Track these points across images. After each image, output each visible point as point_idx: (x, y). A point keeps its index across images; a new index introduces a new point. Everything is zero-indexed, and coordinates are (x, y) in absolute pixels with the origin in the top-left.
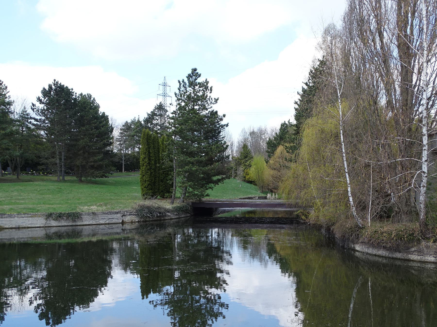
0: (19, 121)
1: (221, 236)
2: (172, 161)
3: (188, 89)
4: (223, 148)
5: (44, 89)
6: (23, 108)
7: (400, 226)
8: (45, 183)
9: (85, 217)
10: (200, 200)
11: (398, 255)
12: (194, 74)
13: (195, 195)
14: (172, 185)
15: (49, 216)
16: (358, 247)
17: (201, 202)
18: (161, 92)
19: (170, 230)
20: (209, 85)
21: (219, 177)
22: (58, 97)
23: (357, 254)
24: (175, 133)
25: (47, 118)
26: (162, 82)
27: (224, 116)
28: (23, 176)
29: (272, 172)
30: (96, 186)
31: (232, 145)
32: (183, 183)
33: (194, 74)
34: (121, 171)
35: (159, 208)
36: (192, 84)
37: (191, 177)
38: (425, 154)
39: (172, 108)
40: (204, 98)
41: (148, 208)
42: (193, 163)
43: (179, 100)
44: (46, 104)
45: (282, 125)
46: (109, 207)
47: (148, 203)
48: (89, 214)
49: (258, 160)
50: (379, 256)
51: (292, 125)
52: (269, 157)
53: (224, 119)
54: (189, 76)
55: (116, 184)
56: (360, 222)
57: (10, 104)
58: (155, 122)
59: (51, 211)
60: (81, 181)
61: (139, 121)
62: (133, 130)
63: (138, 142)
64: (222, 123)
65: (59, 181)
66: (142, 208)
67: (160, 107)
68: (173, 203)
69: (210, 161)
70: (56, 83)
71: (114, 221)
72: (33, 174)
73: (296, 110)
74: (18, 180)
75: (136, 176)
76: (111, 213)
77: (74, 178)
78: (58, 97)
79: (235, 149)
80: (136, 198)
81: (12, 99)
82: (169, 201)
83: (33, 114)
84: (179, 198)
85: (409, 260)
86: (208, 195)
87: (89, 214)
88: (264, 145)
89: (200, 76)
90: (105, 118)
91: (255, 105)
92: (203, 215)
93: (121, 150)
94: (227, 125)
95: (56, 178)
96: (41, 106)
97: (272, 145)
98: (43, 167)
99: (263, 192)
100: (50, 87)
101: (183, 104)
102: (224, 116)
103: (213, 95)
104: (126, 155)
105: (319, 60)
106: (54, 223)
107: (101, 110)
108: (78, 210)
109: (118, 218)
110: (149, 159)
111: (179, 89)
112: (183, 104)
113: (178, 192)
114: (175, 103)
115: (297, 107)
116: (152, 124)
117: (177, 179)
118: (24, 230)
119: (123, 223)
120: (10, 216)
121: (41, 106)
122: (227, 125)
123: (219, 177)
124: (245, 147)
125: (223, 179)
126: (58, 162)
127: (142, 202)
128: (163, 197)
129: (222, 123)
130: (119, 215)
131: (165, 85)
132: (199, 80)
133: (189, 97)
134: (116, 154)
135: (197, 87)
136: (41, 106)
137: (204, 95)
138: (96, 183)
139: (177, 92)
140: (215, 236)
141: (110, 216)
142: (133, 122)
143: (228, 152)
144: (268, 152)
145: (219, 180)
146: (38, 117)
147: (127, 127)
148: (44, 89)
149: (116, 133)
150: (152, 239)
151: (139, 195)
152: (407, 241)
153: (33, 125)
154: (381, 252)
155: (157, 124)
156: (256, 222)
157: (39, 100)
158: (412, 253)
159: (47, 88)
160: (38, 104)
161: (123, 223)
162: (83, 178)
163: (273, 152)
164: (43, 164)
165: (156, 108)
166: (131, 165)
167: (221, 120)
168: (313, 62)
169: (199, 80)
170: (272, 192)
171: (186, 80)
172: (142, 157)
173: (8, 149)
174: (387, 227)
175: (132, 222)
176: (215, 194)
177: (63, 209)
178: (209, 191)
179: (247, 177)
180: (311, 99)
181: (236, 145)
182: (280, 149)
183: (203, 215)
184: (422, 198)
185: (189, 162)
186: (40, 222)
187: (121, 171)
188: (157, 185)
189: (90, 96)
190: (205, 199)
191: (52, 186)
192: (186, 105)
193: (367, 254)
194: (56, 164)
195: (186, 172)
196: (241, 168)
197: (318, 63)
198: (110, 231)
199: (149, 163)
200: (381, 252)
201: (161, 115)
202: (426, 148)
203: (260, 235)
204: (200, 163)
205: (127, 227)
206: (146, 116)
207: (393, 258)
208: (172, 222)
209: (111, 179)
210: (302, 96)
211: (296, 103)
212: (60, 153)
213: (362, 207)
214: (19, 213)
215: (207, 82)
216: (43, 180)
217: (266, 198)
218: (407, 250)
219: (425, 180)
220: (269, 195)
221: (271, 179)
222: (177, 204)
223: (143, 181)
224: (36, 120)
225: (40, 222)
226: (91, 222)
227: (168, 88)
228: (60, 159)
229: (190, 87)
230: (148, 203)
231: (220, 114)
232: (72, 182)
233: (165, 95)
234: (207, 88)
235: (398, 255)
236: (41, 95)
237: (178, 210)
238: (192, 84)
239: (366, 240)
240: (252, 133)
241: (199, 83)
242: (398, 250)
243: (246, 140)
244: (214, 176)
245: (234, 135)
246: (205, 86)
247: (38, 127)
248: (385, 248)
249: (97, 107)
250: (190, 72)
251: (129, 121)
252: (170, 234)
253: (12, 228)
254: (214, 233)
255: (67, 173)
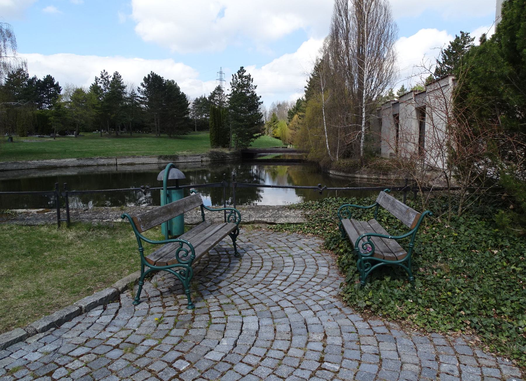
0: (130, 99)
1: (259, 172)
2: (229, 125)
3: (238, 80)
4: (260, 116)
5: (145, 77)
6: (132, 90)
7: (352, 161)
8: (148, 139)
9: (180, 158)
10: (246, 148)
11: (350, 175)
12: (242, 70)
13: (243, 145)
14: (229, 140)
15: (160, 157)
16: (331, 172)
17: (247, 150)
18: (219, 78)
19: (229, 166)
20: (251, 77)
21: (258, 134)
22: (154, 82)
23: (331, 175)
24: (230, 108)
25: (148, 97)
26: (219, 71)
27: (260, 97)
28: (134, 134)
29: (291, 131)
30: (180, 140)
31: (265, 113)
32: (236, 138)
33: (242, 70)
34: (194, 130)
35: (222, 153)
36: (240, 77)
37: (240, 134)
38: (364, 122)
39: (227, 90)
40: (248, 85)
41: (216, 153)
42: (241, 126)
43: (233, 87)
44: (147, 88)
45: (298, 101)
46: (196, 151)
47: (215, 150)
48: (182, 156)
49: (283, 123)
50: (341, 176)
51: (303, 101)
52: (289, 121)
53: (261, 99)
54: (239, 72)
55: (192, 139)
56: (332, 158)
57: (124, 87)
58: (215, 98)
59: (161, 154)
60: (171, 137)
61: (205, 97)
62: (202, 104)
63: (205, 112)
64: (259, 101)
65: (158, 137)
66: (213, 153)
67: (219, 89)
68: (230, 150)
69: (253, 125)
70: (152, 74)
71: (197, 160)
72: (139, 133)
73: (306, 91)
74: (131, 137)
75: (206, 135)
76: (195, 156)
77: (166, 135)
78: (154, 82)
79: (267, 116)
80: (207, 147)
81: (125, 84)
82: (227, 149)
83: (139, 94)
84: (234, 147)
85: (355, 177)
86: (251, 145)
87: (182, 156)
88: (286, 114)
89: (245, 71)
90: (183, 96)
91: (281, 84)
92: (248, 157)
93: (194, 117)
94: (262, 103)
95: (155, 135)
96: (144, 89)
97: (291, 114)
98: (146, 128)
99: (285, 144)
100: (149, 75)
101: (235, 89)
102: (260, 97)
103: (253, 84)
104: (197, 120)
105: (321, 60)
106: (163, 161)
107: (181, 90)
108: (176, 154)
109: (199, 159)
110: (215, 124)
111: (233, 80)
112: (235, 89)
113: (233, 143)
114: (231, 89)
115: (306, 89)
116: (213, 100)
117: (233, 136)
118: (147, 165)
119: (202, 161)
120: (138, 157)
121: (144, 89)
122: (262, 103)
123: (258, 134)
124: (274, 115)
125: (260, 135)
126: (156, 124)
127: (212, 150)
128: (224, 147)
129: (259, 101)
130: (199, 157)
131: (221, 73)
132: (245, 74)
133: (239, 85)
134: (191, 120)
135: (243, 79)
136: (144, 89)
137: (248, 83)
138: (180, 138)
139: (232, 82)
140: (255, 172)
141: (194, 158)
142: (201, 98)
143: (263, 119)
144: (288, 118)
145: (257, 137)
146: (142, 96)
147: (197, 102)
148: (145, 77)
149: (190, 106)
150: (219, 170)
151: (209, 145)
152: (354, 168)
153: (139, 101)
154: (341, 174)
155: (217, 100)
156: (278, 162)
157: (142, 85)
158: (356, 174)
159: (147, 77)
160: (141, 87)
161: (202, 161)
162: (172, 135)
163: (292, 118)
164: (146, 126)
165: (216, 89)
166: (202, 126)
167: (259, 99)
168: (317, 60)
169: (245, 74)
170: (291, 144)
171: (237, 74)
172: (210, 122)
173: (125, 117)
174: (347, 161)
175: (207, 161)
176: (255, 144)
177: (167, 153)
178: (251, 143)
179: (275, 135)
180: (313, 87)
181: (268, 113)
182: (296, 116)
183: (248, 157)
184: (362, 145)
185: (240, 126)
186: (155, 160)
187: (194, 130)
188: (220, 139)
189: (173, 82)
190: (249, 148)
191: (154, 140)
192: (237, 90)
193: (335, 175)
194: (155, 126)
195: (238, 131)
196: (272, 128)
197: (320, 62)
198: (194, 166)
199: (215, 126)
200: (341, 174)
201: (219, 94)
202: (364, 119)
203: (283, 170)
204: (246, 126)
205: (204, 163)
206: (210, 95)
207: (347, 177)
208: (230, 161)
209: (189, 136)
210: (310, 83)
211: (306, 87)
212: (157, 119)
213: (333, 150)
214: (143, 156)
215: (250, 76)
216: (147, 137)
217: (287, 148)
218: (354, 172)
219: (363, 136)
220: (289, 146)
221: (290, 136)
222: (232, 151)
223: (211, 137)
224: (141, 98)
225: (155, 160)
226: (183, 161)
227: (223, 75)
228: (157, 123)
229: (239, 78)
230: (215, 150)
231: (258, 95)
232: (165, 137)
233: (221, 80)
234: (250, 79)
235: (350, 175)
236: (143, 82)
237: (234, 154)
238: (240, 77)
239: (335, 168)
240: (279, 106)
241: (245, 76)
242: (349, 172)
243: (274, 110)
244: (255, 134)
245: (266, 107)
246: (249, 78)
247: (142, 102)
248: (343, 171)
249: (178, 89)
250: (239, 69)
251: (199, 98)
252: (228, 168)
253: (140, 164)
254: (254, 169)
255: (161, 132)
